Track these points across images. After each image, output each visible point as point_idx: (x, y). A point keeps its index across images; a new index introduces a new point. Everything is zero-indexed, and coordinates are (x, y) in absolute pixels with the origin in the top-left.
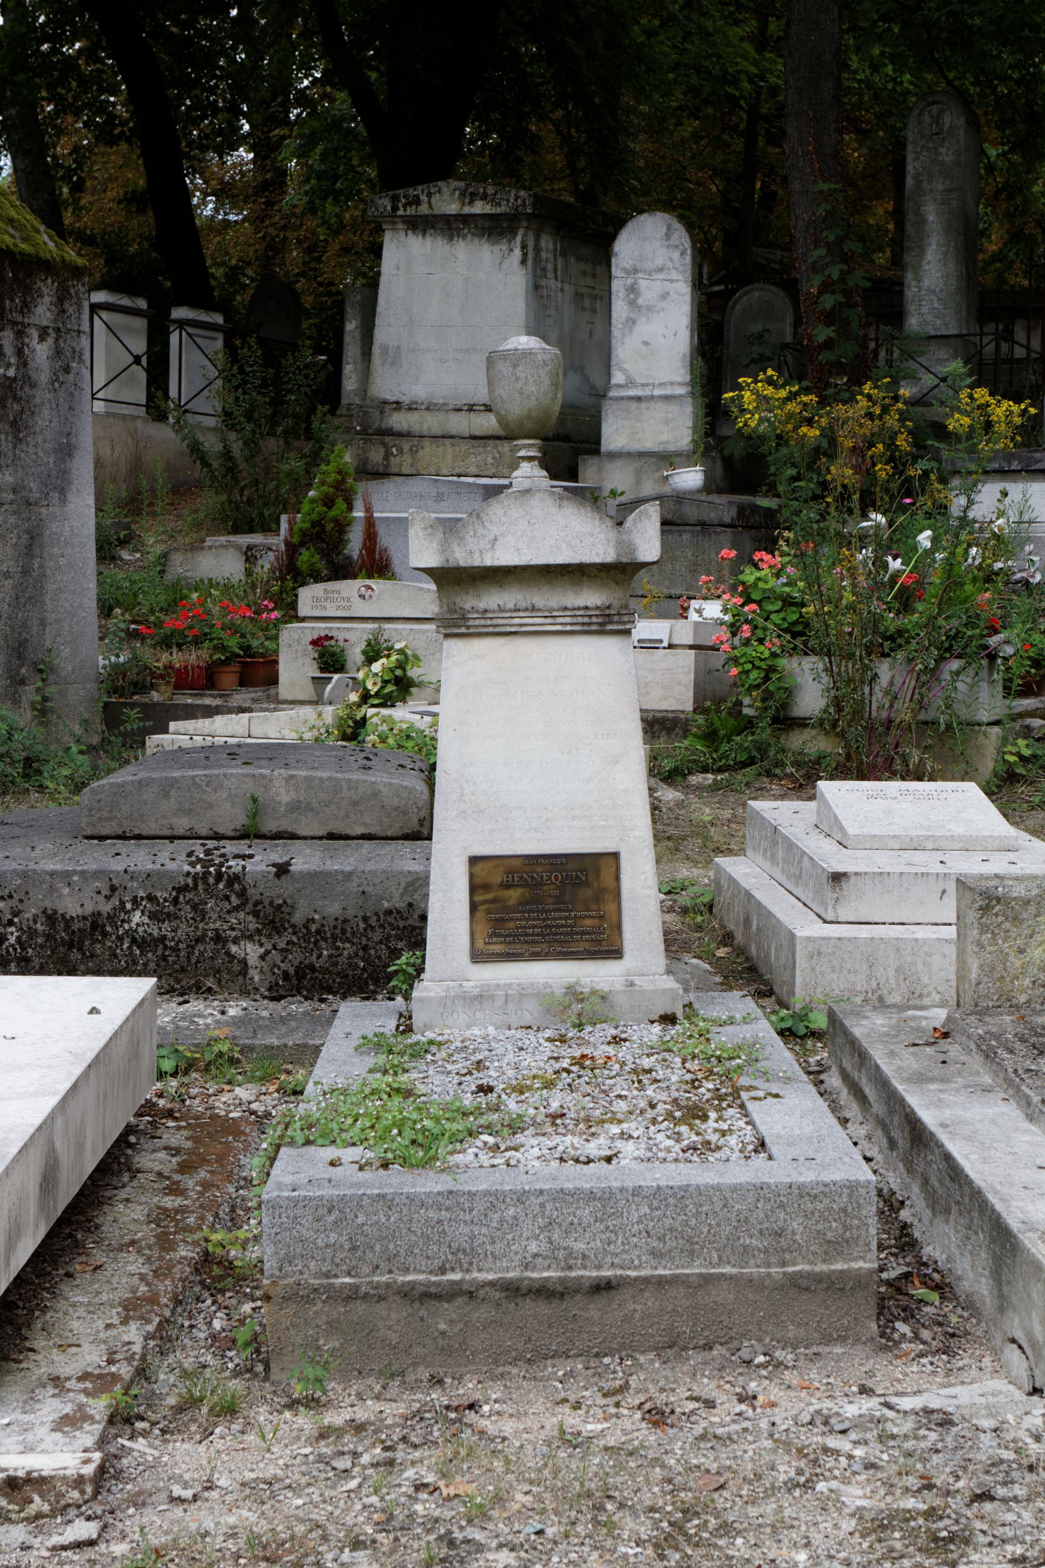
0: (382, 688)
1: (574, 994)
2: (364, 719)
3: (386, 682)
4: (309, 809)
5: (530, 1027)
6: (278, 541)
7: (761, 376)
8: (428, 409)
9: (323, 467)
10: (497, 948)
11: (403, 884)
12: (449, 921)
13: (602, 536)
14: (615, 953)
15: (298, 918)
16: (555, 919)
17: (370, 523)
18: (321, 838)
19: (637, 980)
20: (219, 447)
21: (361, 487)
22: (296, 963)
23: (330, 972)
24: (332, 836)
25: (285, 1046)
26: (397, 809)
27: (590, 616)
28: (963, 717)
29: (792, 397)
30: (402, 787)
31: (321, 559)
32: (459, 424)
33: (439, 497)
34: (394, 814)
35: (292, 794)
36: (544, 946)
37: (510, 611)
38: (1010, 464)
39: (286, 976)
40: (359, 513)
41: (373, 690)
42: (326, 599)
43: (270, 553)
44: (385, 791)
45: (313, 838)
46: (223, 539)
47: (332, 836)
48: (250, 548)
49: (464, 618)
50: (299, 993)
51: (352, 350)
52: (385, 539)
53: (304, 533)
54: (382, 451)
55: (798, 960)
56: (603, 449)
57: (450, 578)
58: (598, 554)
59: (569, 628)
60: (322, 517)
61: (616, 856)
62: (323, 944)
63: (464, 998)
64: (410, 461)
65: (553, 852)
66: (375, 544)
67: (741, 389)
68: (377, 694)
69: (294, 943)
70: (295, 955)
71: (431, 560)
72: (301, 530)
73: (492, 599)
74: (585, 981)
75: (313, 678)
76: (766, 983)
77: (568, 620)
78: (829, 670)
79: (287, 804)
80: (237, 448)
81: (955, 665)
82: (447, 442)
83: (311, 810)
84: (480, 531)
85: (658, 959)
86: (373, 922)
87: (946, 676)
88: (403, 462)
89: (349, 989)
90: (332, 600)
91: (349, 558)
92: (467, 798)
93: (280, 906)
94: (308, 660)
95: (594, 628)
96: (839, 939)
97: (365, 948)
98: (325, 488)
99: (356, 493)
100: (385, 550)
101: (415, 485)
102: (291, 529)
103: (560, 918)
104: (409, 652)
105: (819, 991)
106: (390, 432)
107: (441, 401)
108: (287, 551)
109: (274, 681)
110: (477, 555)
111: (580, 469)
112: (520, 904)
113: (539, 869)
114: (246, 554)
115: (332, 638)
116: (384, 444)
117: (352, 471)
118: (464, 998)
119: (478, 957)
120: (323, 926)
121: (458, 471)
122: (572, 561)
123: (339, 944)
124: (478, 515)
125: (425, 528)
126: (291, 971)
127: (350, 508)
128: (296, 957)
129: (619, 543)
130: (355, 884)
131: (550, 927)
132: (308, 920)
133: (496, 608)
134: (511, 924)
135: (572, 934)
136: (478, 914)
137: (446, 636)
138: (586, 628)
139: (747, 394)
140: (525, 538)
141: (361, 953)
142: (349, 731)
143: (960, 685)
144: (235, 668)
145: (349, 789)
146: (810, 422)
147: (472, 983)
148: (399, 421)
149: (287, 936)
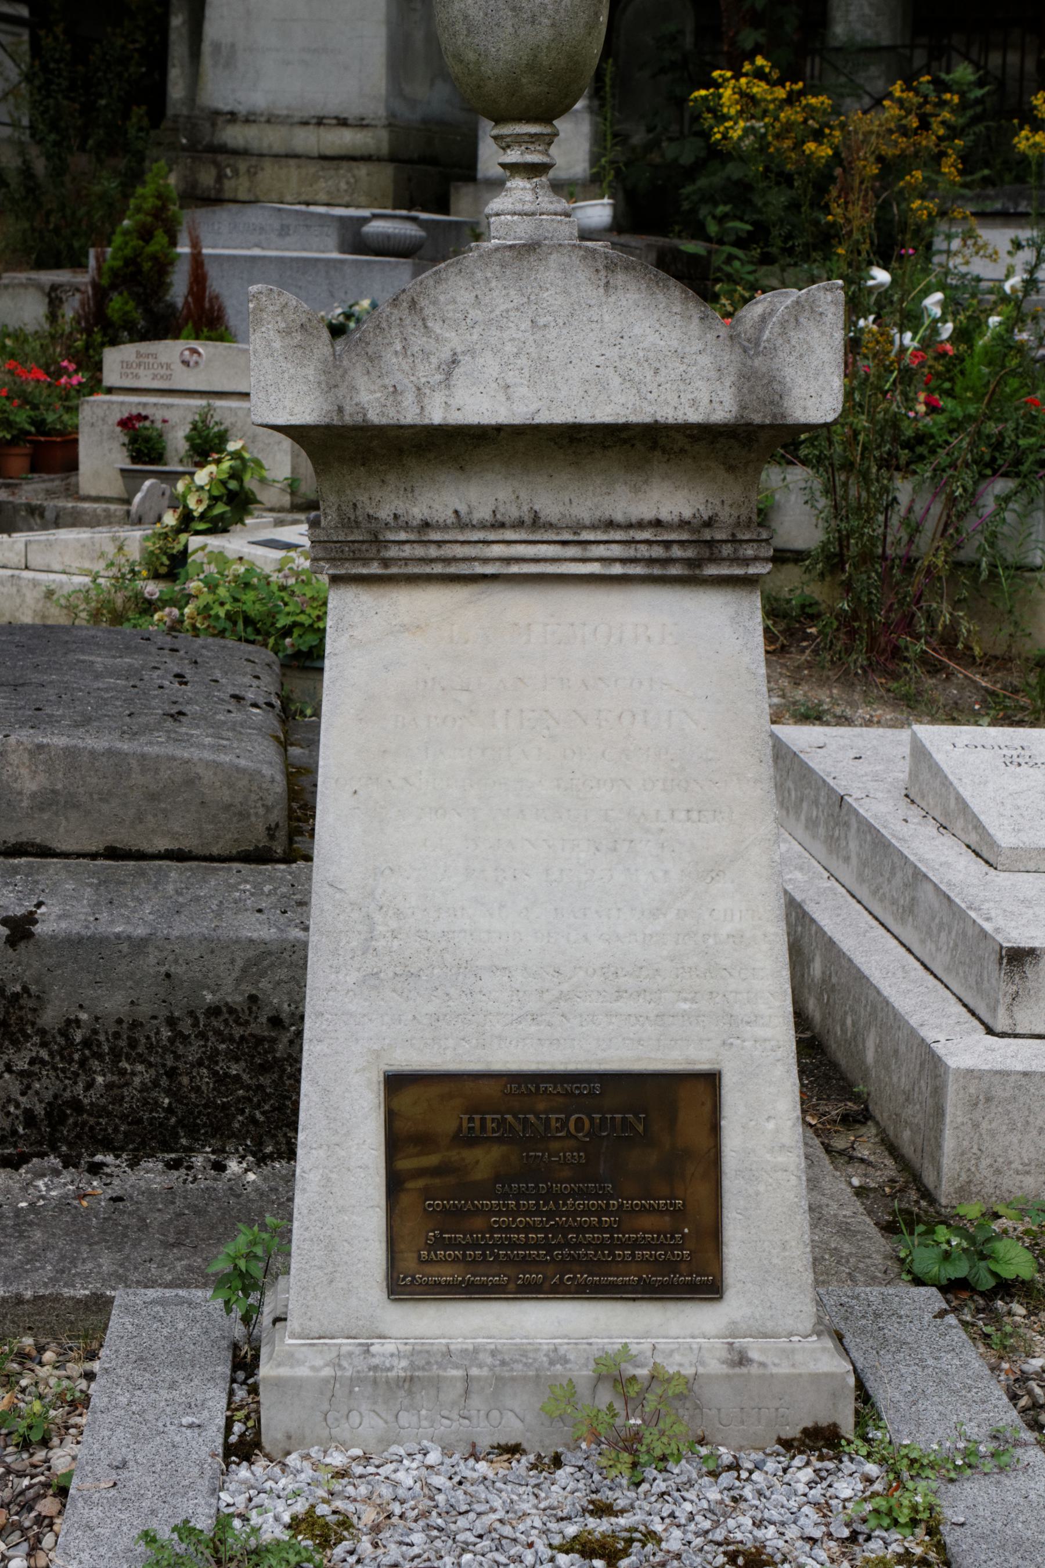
0: (210, 507)
1: (614, 1375)
2: (184, 553)
3: (214, 499)
4: (72, 804)
5: (514, 1450)
6: (83, 279)
7: (747, 67)
8: (268, 121)
9: (140, 190)
10: (447, 1274)
11: (240, 963)
12: (342, 1210)
13: (705, 360)
14: (709, 1287)
15: (50, 1017)
16: (575, 1213)
17: (197, 261)
18: (94, 856)
19: (755, 1350)
20: (17, 162)
21: (186, 217)
22: (48, 1096)
23: (109, 1114)
24: (113, 853)
25: (19, 1300)
26: (228, 807)
27: (667, 544)
28: (1010, 560)
29: (791, 99)
30: (237, 769)
31: (136, 308)
32: (306, 140)
33: (284, 231)
34: (223, 817)
35: (42, 778)
36: (550, 1269)
37: (483, 526)
38: (1017, 205)
39: (29, 1117)
40: (184, 249)
41: (198, 509)
42: (139, 365)
43: (78, 296)
44: (208, 776)
45: (79, 855)
46: (22, 276)
47: (113, 853)
48: (54, 287)
49: (377, 541)
50: (54, 1149)
51: (178, 51)
52: (217, 283)
53: (114, 273)
54: (213, 172)
55: (949, 1110)
56: (480, 175)
57: (343, 449)
58: (694, 403)
59: (617, 569)
60: (138, 253)
61: (711, 1080)
62: (95, 1065)
63: (375, 1382)
64: (247, 184)
65: (572, 1067)
66: (203, 289)
67: (718, 86)
68: (203, 517)
69: (43, 1062)
70: (45, 1081)
71: (305, 409)
72: (111, 269)
73: (443, 497)
74: (640, 1347)
75: (122, 471)
76: (857, 1098)
77: (616, 551)
78: (829, 490)
79: (33, 796)
80: (40, 166)
81: (1001, 486)
82: (292, 162)
83: (76, 806)
84: (418, 341)
85: (798, 1309)
86: (186, 1027)
87: (989, 504)
88: (241, 187)
89: (143, 1144)
90: (147, 367)
91: (172, 306)
92: (381, 944)
93: (16, 996)
94: (116, 445)
95: (674, 570)
96: (1025, 1074)
97: (172, 1073)
98: (140, 217)
99: (180, 224)
100: (217, 297)
101: (254, 216)
102: (99, 268)
103: (587, 1212)
104: (247, 455)
105: (985, 1162)
106: (223, 149)
107: (285, 112)
108: (95, 294)
109: (72, 466)
110: (409, 399)
111: (453, 199)
112: (497, 1178)
113: (541, 1106)
114: (49, 295)
115: (146, 418)
116: (216, 164)
117: (174, 195)
118: (375, 1382)
119: (401, 1286)
120: (95, 1032)
121: (304, 198)
122: (634, 419)
123: (124, 1064)
124: (413, 304)
125: (287, 332)
126: (39, 1110)
127: (174, 243)
128: (46, 1085)
129: (747, 377)
130: (152, 960)
131: (565, 1230)
132: (68, 1022)
133: (451, 519)
134: (478, 1222)
135: (612, 1247)
136: (405, 1200)
137: (335, 580)
138: (657, 571)
139: (727, 93)
140: (523, 361)
141: (164, 1082)
142: (163, 570)
143: (1009, 516)
144: (26, 449)
145: (143, 771)
146: (818, 136)
147: (390, 1346)
148: (234, 135)
149: (32, 1049)
